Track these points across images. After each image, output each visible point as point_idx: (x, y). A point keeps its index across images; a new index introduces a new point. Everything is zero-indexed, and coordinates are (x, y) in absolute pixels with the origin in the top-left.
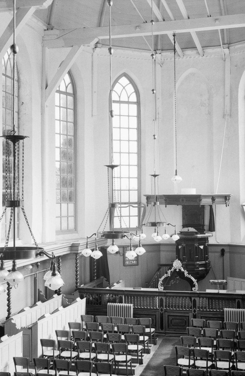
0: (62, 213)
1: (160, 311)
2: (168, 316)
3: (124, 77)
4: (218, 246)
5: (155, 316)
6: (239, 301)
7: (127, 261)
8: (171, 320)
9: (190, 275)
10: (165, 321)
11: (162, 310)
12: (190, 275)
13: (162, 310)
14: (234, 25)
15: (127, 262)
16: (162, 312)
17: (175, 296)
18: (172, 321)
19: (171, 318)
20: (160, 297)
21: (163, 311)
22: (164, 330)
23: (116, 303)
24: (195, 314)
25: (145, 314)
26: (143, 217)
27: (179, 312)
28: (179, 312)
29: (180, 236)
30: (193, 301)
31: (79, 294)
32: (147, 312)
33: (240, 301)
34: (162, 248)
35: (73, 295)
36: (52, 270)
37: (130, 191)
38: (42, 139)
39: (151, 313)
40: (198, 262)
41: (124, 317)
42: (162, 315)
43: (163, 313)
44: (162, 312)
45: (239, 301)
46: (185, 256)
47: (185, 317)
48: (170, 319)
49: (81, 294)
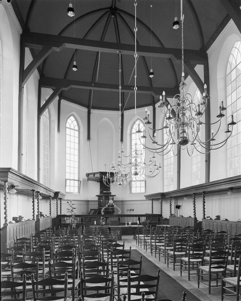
20: (119, 217)
29: (111, 194)
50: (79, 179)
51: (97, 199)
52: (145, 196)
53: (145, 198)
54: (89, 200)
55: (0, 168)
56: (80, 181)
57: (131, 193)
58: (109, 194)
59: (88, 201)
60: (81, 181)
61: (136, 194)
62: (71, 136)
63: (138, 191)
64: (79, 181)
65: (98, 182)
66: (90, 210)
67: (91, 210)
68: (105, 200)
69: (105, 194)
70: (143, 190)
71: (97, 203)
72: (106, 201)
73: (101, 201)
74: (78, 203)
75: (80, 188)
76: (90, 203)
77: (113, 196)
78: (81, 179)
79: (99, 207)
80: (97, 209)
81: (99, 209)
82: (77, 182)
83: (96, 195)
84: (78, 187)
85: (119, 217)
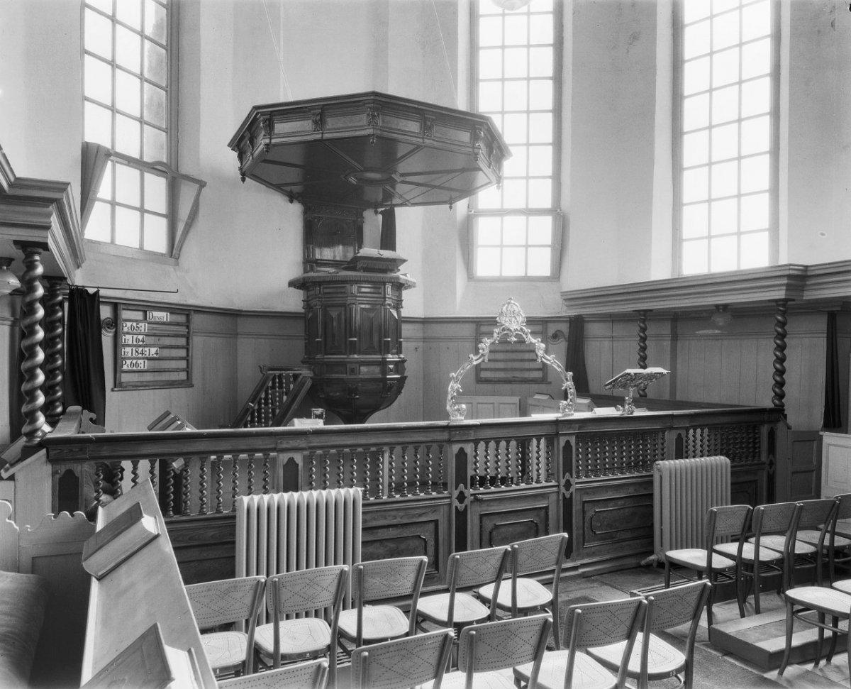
0: (292, 161)
1: (456, 503)
2: (482, 516)
4: (459, 322)
6: (291, 460)
7: (129, 346)
9: (571, 373)
10: (472, 536)
12: (571, 373)
15: (128, 350)
16: (463, 505)
17: (399, 444)
18: (494, 533)
19: (590, 513)
21: (467, 502)
23: (324, 489)
25: (395, 522)
30: (564, 447)
31: (48, 469)
32: (401, 513)
33: (573, 440)
34: (197, 320)
35: (12, 478)
36: (151, 330)
37: (531, 181)
39: (420, 515)
40: (356, 356)
41: (353, 562)
43: (466, 506)
44: (461, 507)
45: (462, 450)
46: (355, 337)
47: (535, 513)
49: (62, 469)
57: (470, 275)
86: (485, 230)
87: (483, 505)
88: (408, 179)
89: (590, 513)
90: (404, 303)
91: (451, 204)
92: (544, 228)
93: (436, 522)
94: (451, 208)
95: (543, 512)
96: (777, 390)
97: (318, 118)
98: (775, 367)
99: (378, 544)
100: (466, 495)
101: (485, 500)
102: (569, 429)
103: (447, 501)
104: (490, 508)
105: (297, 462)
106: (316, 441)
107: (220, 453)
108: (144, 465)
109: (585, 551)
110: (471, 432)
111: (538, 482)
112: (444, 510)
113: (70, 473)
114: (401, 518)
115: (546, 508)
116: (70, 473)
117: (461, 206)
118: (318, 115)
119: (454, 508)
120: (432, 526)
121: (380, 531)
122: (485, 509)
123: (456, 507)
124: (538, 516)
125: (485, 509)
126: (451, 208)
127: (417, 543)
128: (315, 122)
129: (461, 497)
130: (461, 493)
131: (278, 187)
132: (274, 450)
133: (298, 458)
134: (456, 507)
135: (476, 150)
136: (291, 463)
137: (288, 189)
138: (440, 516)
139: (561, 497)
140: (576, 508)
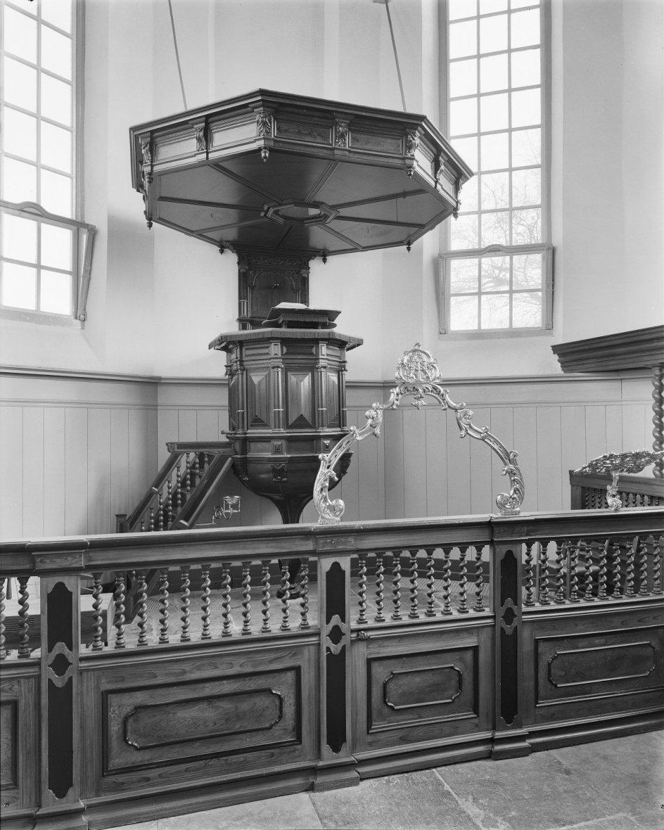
2: (370, 662)
3: (70, 40)
5: (542, 647)
6: (336, 566)
8: (385, 685)
11: (336, 635)
13: (336, 635)
14: (560, 39)
16: (340, 646)
18: (391, 686)
19: (380, 672)
20: (53, 581)
21: (345, 641)
22: (345, 748)
24: (509, 630)
26: (86, 281)
27: (400, 638)
28: (400, 638)
29: (335, 330)
38: (64, 128)
42: (337, 664)
43: (344, 647)
44: (336, 649)
45: (336, 566)
47: (457, 655)
48: (381, 682)
50: (83, 216)
51: (216, 365)
52: (557, 349)
53: (554, 366)
54: (162, 377)
55: (1, 546)
56: (86, 226)
57: (443, 331)
58: (315, 325)
59: (150, 385)
60: (93, 233)
61: (479, 335)
62: (34, 110)
63: (495, 315)
64: (77, 225)
65: (222, 252)
66: (164, 456)
67: (178, 449)
68: (286, 370)
69: (291, 325)
70: (529, 313)
71: (222, 397)
72: (293, 378)
73: (256, 378)
74: (74, 397)
75: (89, 272)
76: (166, 396)
77: (342, 344)
78: (97, 219)
79: (232, 427)
80: (224, 439)
81: (238, 446)
82: (66, 235)
83: (214, 336)
84: (75, 273)
85: (53, 581)
86: (461, 272)
87: (371, 646)
88: (344, 212)
89: (546, 658)
90: (348, 366)
91: (409, 244)
92: (532, 270)
93: (297, 670)
94: (409, 249)
95: (469, 656)
96: (657, 473)
97: (202, 134)
98: (654, 423)
99: (204, 705)
100: (516, 613)
101: (372, 639)
102: (512, 534)
103: (32, 671)
104: (382, 650)
105: (343, 568)
106: (101, 558)
107: (463, 547)
108: (34, 583)
109: (539, 712)
110: (350, 539)
111: (528, 604)
112: (308, 654)
113: (60, 587)
114: (241, 666)
115: (475, 649)
116: (60, 587)
117: (428, 242)
118: (201, 130)
119: (325, 649)
120: (290, 676)
121: (207, 685)
122: (372, 650)
123: (328, 649)
124: (462, 660)
125: (372, 650)
126: (409, 249)
127: (267, 702)
128: (199, 140)
129: (61, 664)
130: (337, 628)
131: (200, 234)
132: (313, 553)
133: (345, 563)
134: (328, 649)
135: (407, 162)
136: (336, 569)
137: (215, 235)
138: (305, 661)
139: (325, 654)
140: (525, 646)
